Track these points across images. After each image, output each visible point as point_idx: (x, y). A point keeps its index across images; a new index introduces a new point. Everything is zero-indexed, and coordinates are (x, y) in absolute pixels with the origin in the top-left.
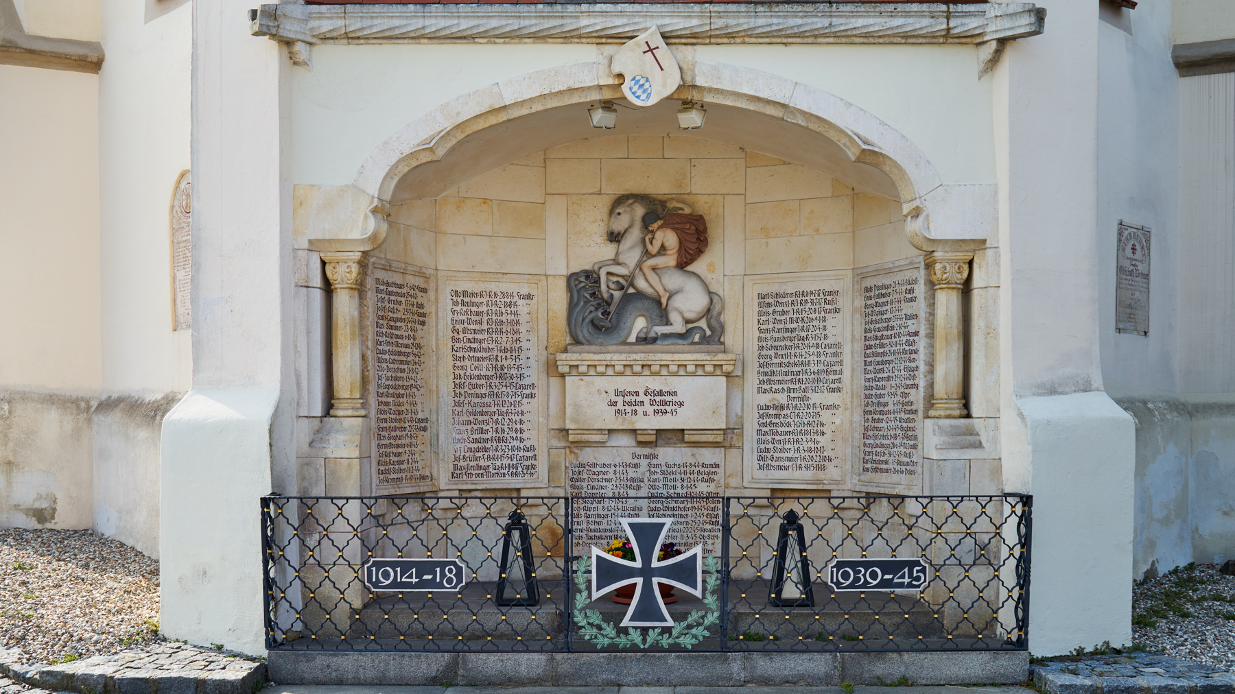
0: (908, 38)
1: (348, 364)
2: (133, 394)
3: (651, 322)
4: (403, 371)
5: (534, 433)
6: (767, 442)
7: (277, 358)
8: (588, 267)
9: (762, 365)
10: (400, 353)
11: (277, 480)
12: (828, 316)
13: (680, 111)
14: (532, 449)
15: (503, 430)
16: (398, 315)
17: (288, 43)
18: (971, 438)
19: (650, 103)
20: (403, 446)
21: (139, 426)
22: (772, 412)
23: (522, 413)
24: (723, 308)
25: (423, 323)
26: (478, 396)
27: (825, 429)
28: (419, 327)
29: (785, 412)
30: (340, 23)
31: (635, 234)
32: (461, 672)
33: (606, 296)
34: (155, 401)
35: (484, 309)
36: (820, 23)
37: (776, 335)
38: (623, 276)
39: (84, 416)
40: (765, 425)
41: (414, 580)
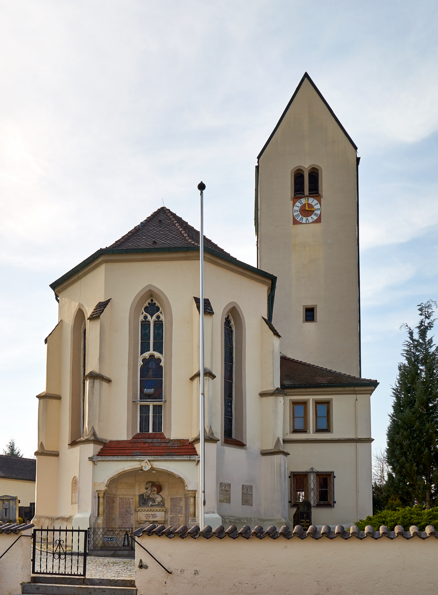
0: (184, 460)
1: (101, 509)
2: (63, 516)
3: (153, 503)
4: (110, 510)
5: (133, 521)
6: (171, 523)
7: (91, 508)
8: (142, 494)
9: (171, 510)
10: (110, 508)
11: (90, 526)
12: (181, 502)
13: (152, 471)
14: (132, 524)
15: (127, 521)
16: (110, 502)
17: (94, 462)
18: (195, 520)
19: (146, 470)
20: (110, 522)
21: (64, 522)
22: (172, 518)
23: (131, 518)
24: (165, 500)
25: (114, 503)
26: (123, 515)
27: (180, 521)
28: (113, 503)
29: (174, 518)
30: (102, 459)
31: (150, 488)
32: (116, 554)
33: (145, 498)
34: (68, 517)
35: (124, 500)
36: (171, 459)
37: (173, 505)
38: (148, 495)
39: (53, 521)
40: (171, 520)
41: (110, 540)
